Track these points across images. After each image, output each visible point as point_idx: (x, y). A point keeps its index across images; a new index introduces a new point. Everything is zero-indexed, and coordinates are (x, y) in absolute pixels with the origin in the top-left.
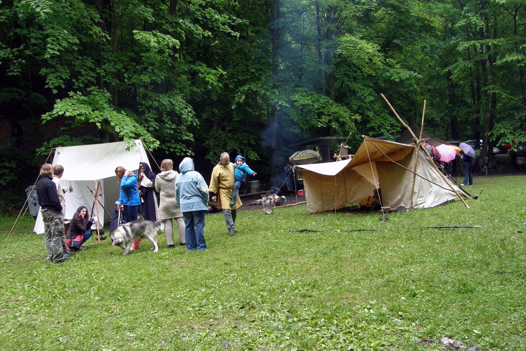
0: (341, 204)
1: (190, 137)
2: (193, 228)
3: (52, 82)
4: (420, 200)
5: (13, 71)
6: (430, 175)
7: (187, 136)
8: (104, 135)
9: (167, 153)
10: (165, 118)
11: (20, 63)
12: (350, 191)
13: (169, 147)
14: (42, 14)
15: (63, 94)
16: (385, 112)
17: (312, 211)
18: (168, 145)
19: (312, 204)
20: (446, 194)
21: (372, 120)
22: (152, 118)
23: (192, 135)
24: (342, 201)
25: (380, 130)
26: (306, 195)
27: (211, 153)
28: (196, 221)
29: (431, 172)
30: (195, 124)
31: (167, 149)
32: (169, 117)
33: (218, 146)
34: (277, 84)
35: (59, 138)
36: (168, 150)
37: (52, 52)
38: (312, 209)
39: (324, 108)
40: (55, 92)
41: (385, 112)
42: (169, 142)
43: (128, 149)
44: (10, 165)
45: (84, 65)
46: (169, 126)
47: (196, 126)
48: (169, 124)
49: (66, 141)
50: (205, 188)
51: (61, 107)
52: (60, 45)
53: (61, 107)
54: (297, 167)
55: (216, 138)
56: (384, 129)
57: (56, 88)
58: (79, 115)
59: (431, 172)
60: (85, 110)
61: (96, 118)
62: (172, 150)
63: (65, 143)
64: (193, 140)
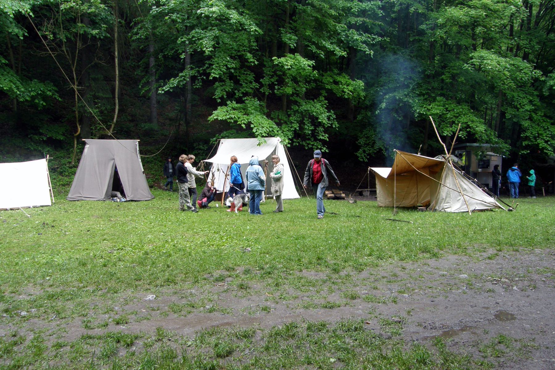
0: (412, 203)
1: (326, 137)
2: (254, 201)
3: (218, 93)
4: (445, 205)
5: (196, 85)
6: (461, 186)
7: (323, 136)
8: (247, 132)
9: (306, 148)
10: (306, 121)
11: (202, 79)
12: (422, 193)
13: (309, 144)
14: (206, 52)
15: (223, 103)
16: (547, 122)
17: (381, 205)
18: (308, 142)
19: (382, 199)
20: (477, 204)
21: (529, 129)
22: (295, 120)
23: (327, 135)
24: (413, 201)
25: (536, 140)
26: (378, 192)
27: (361, 151)
28: (256, 195)
29: (462, 183)
30: (334, 126)
31: (306, 145)
32: (310, 120)
33: (368, 144)
34: (424, 92)
35: (228, 131)
36: (307, 146)
37: (214, 75)
38: (382, 203)
39: (457, 117)
40: (219, 101)
41: (547, 122)
42: (309, 139)
43: (259, 144)
44: (203, 148)
45: (246, 79)
46: (308, 128)
47: (335, 128)
48: (308, 126)
49: (232, 134)
50: (263, 177)
51: (220, 114)
52: (221, 70)
53: (220, 114)
54: (371, 169)
55: (367, 137)
56: (541, 139)
57: (220, 98)
58: (229, 118)
59: (462, 183)
60: (235, 115)
61: (243, 120)
62: (310, 146)
63: (231, 136)
64: (328, 140)
